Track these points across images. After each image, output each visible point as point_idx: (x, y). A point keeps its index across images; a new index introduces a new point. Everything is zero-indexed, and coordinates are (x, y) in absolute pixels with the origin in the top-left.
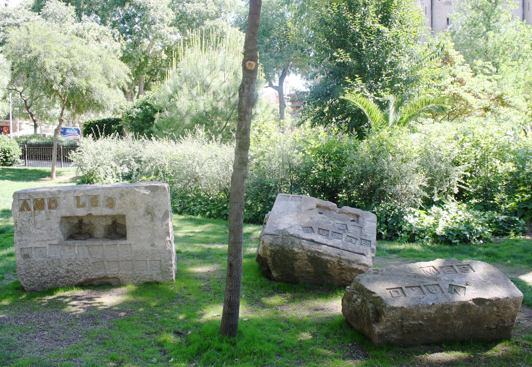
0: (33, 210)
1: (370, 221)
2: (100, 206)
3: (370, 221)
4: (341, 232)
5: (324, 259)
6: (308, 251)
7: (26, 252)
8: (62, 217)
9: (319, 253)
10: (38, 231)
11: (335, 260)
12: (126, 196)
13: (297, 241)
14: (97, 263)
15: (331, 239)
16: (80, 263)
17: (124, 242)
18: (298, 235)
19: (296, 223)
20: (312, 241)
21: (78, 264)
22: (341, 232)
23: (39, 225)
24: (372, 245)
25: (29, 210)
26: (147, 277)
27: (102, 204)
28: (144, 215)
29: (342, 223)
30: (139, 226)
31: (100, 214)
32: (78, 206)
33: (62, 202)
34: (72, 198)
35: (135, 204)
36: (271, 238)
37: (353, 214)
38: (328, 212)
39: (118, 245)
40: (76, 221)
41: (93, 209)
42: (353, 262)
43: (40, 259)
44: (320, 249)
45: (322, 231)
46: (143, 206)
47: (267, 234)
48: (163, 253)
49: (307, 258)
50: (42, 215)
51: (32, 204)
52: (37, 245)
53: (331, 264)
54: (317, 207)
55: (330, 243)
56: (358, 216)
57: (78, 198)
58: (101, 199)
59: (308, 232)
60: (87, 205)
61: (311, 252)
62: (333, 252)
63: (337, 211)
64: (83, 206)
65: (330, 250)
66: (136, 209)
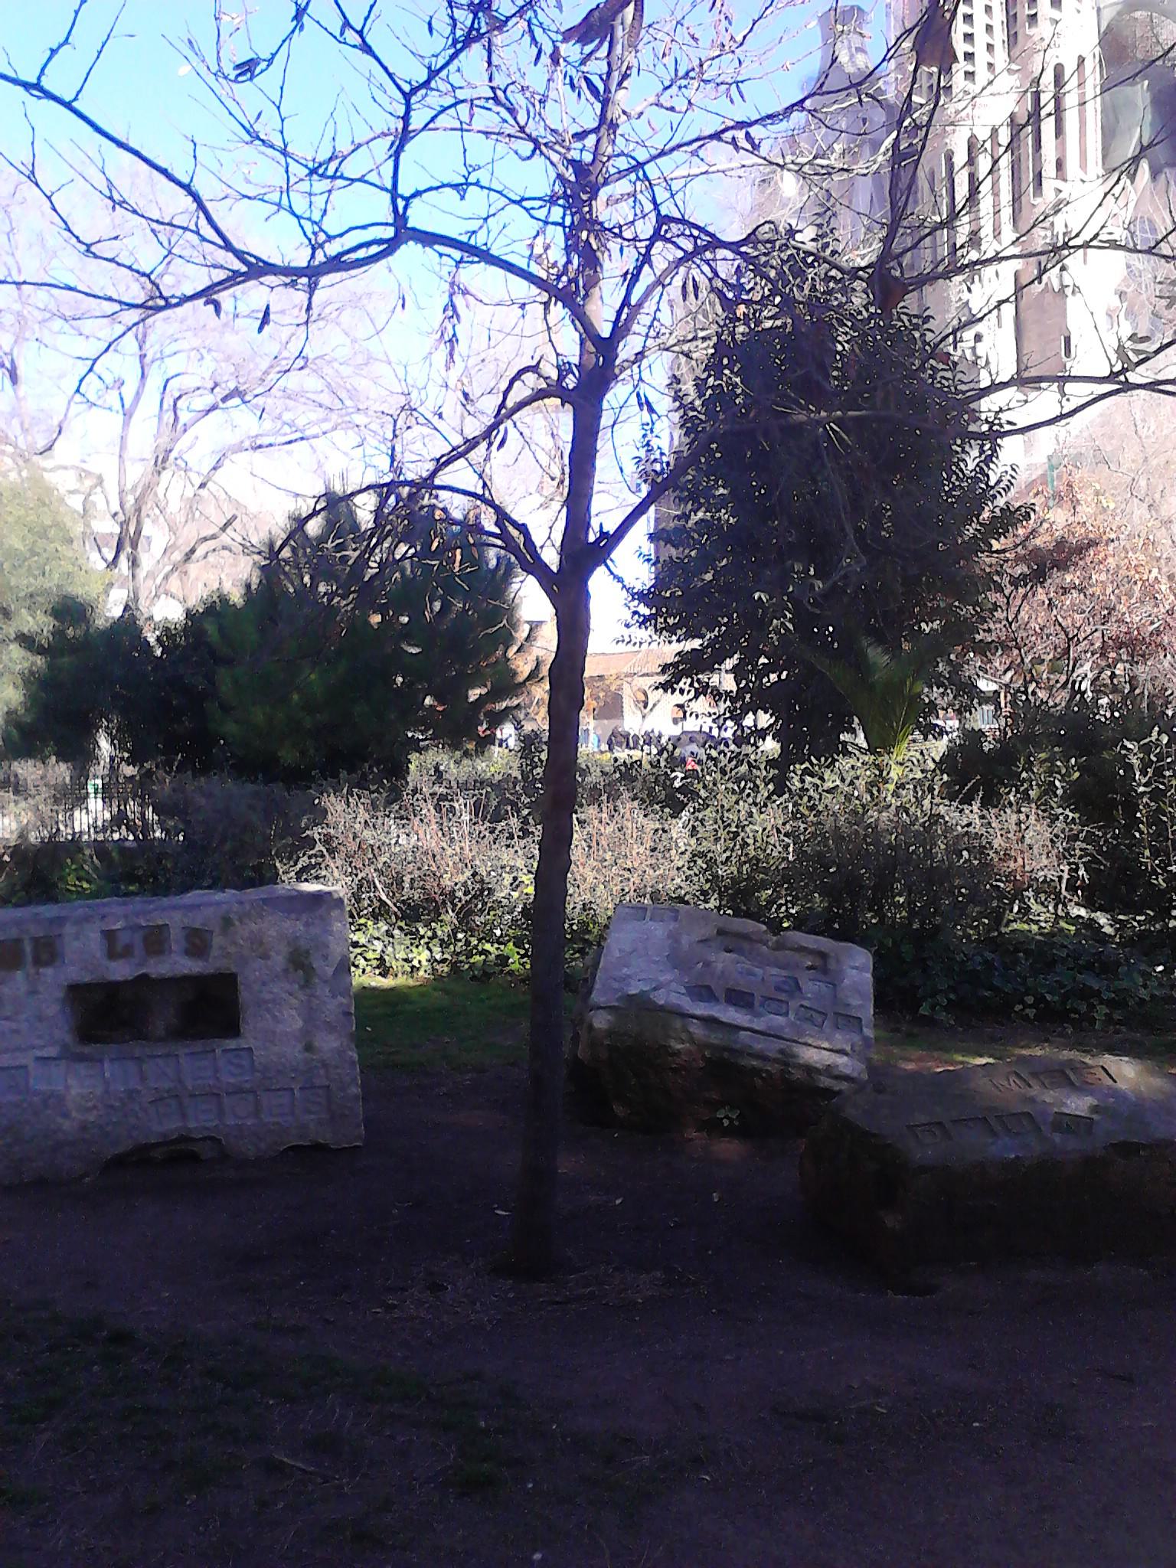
1: (856, 968)
3: (856, 968)
4: (783, 997)
6: (708, 1046)
9: (732, 1051)
13: (678, 1023)
15: (758, 1015)
17: (231, 1044)
22: (783, 997)
28: (286, 971)
30: (274, 1001)
31: (170, 975)
32: (112, 955)
35: (261, 943)
38: (746, 945)
45: (738, 998)
46: (285, 949)
48: (337, 1067)
49: (702, 1064)
53: (762, 1078)
55: (759, 1025)
56: (823, 955)
58: (175, 935)
62: (772, 1047)
64: (127, 952)
65: (760, 1045)
66: (265, 956)
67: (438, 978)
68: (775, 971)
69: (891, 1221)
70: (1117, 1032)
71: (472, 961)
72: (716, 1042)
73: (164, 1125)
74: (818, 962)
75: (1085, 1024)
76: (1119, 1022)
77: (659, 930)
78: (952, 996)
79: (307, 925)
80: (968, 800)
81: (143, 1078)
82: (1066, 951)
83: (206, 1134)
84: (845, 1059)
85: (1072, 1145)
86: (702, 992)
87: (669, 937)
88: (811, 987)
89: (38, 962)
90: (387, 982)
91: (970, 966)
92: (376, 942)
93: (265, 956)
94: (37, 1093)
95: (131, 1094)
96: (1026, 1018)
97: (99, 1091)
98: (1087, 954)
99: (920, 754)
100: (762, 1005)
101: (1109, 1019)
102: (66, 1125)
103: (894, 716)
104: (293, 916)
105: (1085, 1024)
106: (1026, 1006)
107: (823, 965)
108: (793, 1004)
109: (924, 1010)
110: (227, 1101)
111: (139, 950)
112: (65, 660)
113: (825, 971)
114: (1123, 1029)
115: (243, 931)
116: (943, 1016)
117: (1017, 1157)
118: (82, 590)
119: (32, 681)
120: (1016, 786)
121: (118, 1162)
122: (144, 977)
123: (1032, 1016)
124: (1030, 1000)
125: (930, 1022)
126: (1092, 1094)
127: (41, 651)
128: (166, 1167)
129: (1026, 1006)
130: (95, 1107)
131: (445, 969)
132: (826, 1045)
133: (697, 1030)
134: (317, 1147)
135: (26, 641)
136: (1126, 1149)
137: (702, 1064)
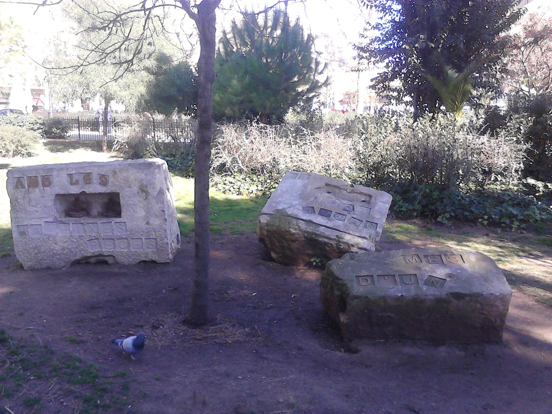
0: (27, 187)
1: (383, 202)
2: (93, 183)
3: (383, 202)
4: (345, 213)
5: (321, 241)
6: (305, 232)
7: (22, 229)
8: (56, 195)
9: (316, 234)
10: (33, 209)
11: (333, 243)
12: (118, 173)
13: (295, 222)
14: (92, 241)
15: (331, 220)
16: (75, 241)
17: (118, 220)
18: (297, 215)
19: (296, 203)
20: (311, 222)
21: (73, 241)
22: (345, 213)
23: (33, 203)
24: (378, 228)
25: (23, 187)
26: (142, 255)
27: (95, 181)
28: (138, 193)
29: (350, 203)
30: (133, 204)
31: (93, 192)
32: (72, 184)
33: (56, 180)
34: (65, 176)
35: (128, 181)
36: (268, 218)
37: (365, 195)
38: (337, 190)
39: (113, 223)
40: (73, 199)
41: (87, 186)
42: (353, 246)
43: (36, 236)
44: (318, 231)
45: (325, 213)
46: (138, 185)
47: (264, 214)
48: (159, 231)
49: (304, 239)
50: (36, 193)
51: (26, 183)
52: (33, 222)
53: (329, 247)
54: (326, 185)
55: (330, 224)
56: (370, 196)
57: (70, 176)
58: (95, 177)
59: (308, 212)
60: (80, 183)
61: (308, 232)
62: (333, 234)
63: (348, 190)
64: (77, 183)
65: (328, 233)
66: (130, 187)
67: (257, 197)
68: (345, 202)
69: (343, 318)
70: (522, 233)
71: (271, 191)
72: (310, 230)
73: (91, 250)
74: (368, 199)
75: (508, 229)
76: (524, 229)
77: (299, 183)
78: (452, 214)
79: (146, 175)
80: (483, 133)
81: (85, 231)
82: (509, 197)
83: (109, 253)
84: (365, 240)
85: (429, 292)
86: (310, 210)
87: (303, 186)
88: (359, 209)
89: (44, 185)
90: (239, 197)
91: (463, 202)
92: (238, 182)
93: (130, 187)
94: (45, 235)
95: (81, 237)
96: (483, 224)
97: (68, 235)
98: (522, 201)
99: (465, 115)
100: (334, 216)
101: (519, 228)
102: (57, 248)
103: (457, 98)
104: (140, 171)
105: (508, 229)
106: (484, 219)
107: (368, 201)
108: (349, 216)
109: (439, 219)
110: (116, 242)
111: (81, 181)
112: (161, 78)
113: (369, 203)
114: (525, 232)
115: (121, 176)
116: (446, 222)
117: (402, 295)
118: (168, 50)
119: (149, 85)
120: (505, 128)
121: (77, 263)
122: (83, 193)
123: (485, 224)
124: (486, 217)
125: (441, 224)
126: (450, 267)
127: (153, 73)
128: (93, 266)
129: (484, 219)
130: (67, 241)
131: (260, 194)
132: (357, 235)
133: (302, 225)
134: (153, 262)
135: (147, 69)
136: (458, 296)
137: (304, 239)
